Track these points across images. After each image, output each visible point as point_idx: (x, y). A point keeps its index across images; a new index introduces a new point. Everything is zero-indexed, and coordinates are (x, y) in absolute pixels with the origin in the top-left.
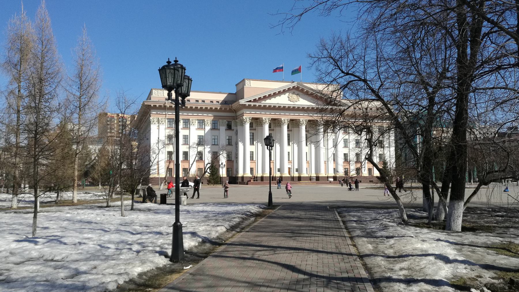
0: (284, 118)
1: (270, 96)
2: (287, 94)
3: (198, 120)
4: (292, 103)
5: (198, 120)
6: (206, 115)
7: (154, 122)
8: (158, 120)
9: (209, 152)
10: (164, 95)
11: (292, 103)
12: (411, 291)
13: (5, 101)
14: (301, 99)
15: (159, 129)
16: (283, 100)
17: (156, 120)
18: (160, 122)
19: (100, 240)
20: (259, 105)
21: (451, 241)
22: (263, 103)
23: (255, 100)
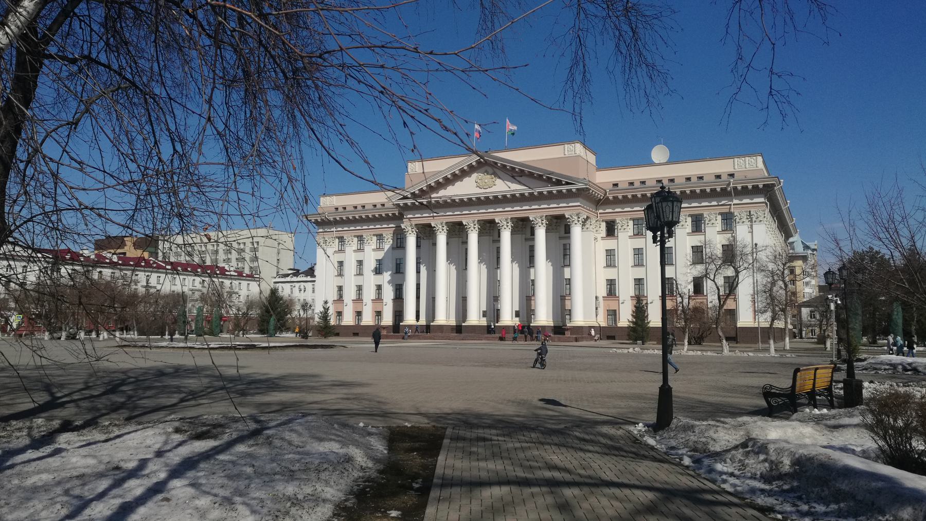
0: (534, 216)
1: (440, 185)
2: (475, 175)
3: (720, 214)
4: (483, 191)
5: (720, 214)
6: (459, 213)
7: (743, 220)
8: (750, 215)
9: (389, 282)
10: (758, 165)
11: (483, 191)
12: (744, 520)
13: (128, 206)
14: (499, 182)
15: (752, 232)
16: (467, 188)
17: (744, 215)
18: (754, 219)
19: (41, 432)
20: (567, 190)
21: (330, 414)
22: (516, 188)
23: (414, 195)
